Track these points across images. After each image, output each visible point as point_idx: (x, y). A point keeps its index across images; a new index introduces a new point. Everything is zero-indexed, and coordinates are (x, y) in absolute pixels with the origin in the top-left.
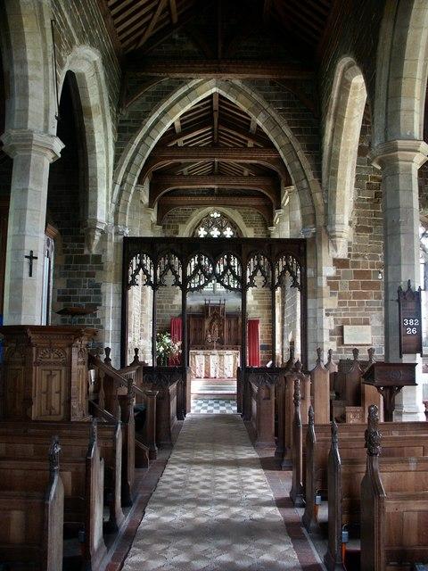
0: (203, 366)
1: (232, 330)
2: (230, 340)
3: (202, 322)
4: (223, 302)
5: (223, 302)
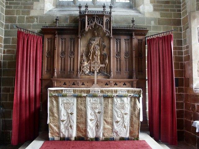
0: (74, 117)
1: (123, 55)
2: (119, 70)
3: (75, 43)
4: (108, 9)
5: (108, 9)
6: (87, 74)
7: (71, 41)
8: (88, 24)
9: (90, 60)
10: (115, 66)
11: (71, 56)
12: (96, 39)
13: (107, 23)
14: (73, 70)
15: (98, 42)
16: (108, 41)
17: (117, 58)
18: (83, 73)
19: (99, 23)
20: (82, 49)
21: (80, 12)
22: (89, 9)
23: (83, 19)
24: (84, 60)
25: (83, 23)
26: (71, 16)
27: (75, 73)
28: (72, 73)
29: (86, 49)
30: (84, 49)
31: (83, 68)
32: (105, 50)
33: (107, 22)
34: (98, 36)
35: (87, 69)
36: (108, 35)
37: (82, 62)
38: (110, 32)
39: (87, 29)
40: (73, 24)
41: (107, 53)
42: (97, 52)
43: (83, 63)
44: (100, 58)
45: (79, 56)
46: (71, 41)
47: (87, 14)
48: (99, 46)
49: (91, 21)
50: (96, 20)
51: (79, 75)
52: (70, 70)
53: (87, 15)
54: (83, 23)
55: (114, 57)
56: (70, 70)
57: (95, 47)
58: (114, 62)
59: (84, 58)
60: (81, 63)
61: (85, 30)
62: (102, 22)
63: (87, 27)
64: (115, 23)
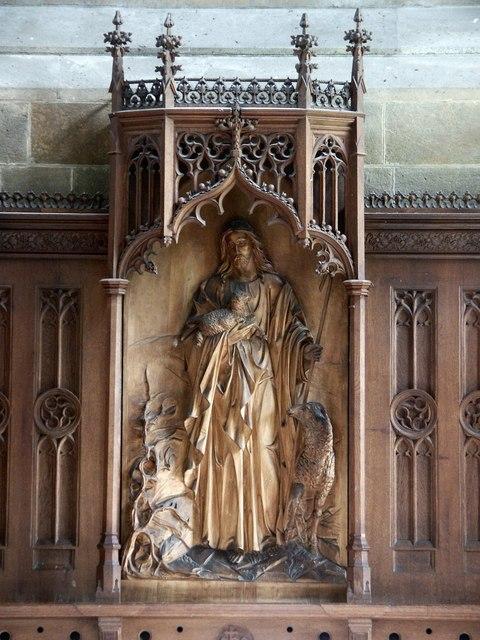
4: (331, 69)
5: (331, 69)
6: (177, 563)
7: (53, 314)
8: (185, 183)
9: (198, 457)
10: (393, 504)
11: (55, 424)
12: (241, 304)
13: (330, 174)
14: (71, 534)
15: (262, 313)
16: (335, 308)
17: (406, 445)
18: (144, 558)
19: (270, 177)
20: (134, 376)
21: (120, 87)
22: (192, 68)
23: (144, 141)
24: (153, 461)
25: (145, 173)
26: (46, 110)
27: (85, 557)
28: (59, 561)
29: (169, 368)
30: (155, 370)
31: (143, 524)
32: (316, 374)
33: (330, 164)
34: (260, 275)
35: (177, 524)
36: (333, 268)
37: (135, 474)
38: (352, 245)
39: (171, 228)
40: (68, 176)
41: (330, 402)
42: (248, 398)
43: (146, 478)
44: (277, 439)
45: (117, 425)
46: (73, 201)
47: (170, 105)
48: (268, 346)
49: (205, 163)
50: (245, 151)
51: (117, 575)
52: (48, 537)
53: (171, 113)
54: (145, 172)
55: (385, 431)
56: (48, 537)
57: (239, 362)
58: (377, 475)
59: (154, 429)
60: (132, 484)
61: (161, 237)
62: (290, 169)
63: (176, 207)
64: (394, 156)
